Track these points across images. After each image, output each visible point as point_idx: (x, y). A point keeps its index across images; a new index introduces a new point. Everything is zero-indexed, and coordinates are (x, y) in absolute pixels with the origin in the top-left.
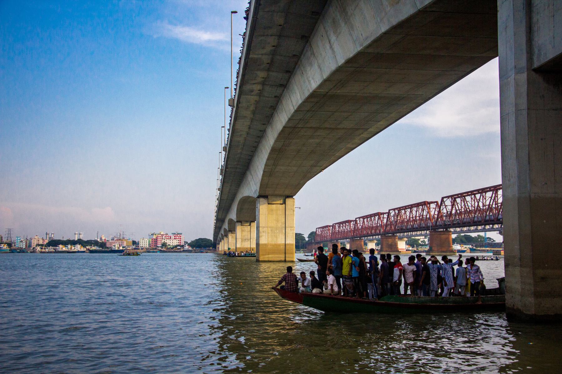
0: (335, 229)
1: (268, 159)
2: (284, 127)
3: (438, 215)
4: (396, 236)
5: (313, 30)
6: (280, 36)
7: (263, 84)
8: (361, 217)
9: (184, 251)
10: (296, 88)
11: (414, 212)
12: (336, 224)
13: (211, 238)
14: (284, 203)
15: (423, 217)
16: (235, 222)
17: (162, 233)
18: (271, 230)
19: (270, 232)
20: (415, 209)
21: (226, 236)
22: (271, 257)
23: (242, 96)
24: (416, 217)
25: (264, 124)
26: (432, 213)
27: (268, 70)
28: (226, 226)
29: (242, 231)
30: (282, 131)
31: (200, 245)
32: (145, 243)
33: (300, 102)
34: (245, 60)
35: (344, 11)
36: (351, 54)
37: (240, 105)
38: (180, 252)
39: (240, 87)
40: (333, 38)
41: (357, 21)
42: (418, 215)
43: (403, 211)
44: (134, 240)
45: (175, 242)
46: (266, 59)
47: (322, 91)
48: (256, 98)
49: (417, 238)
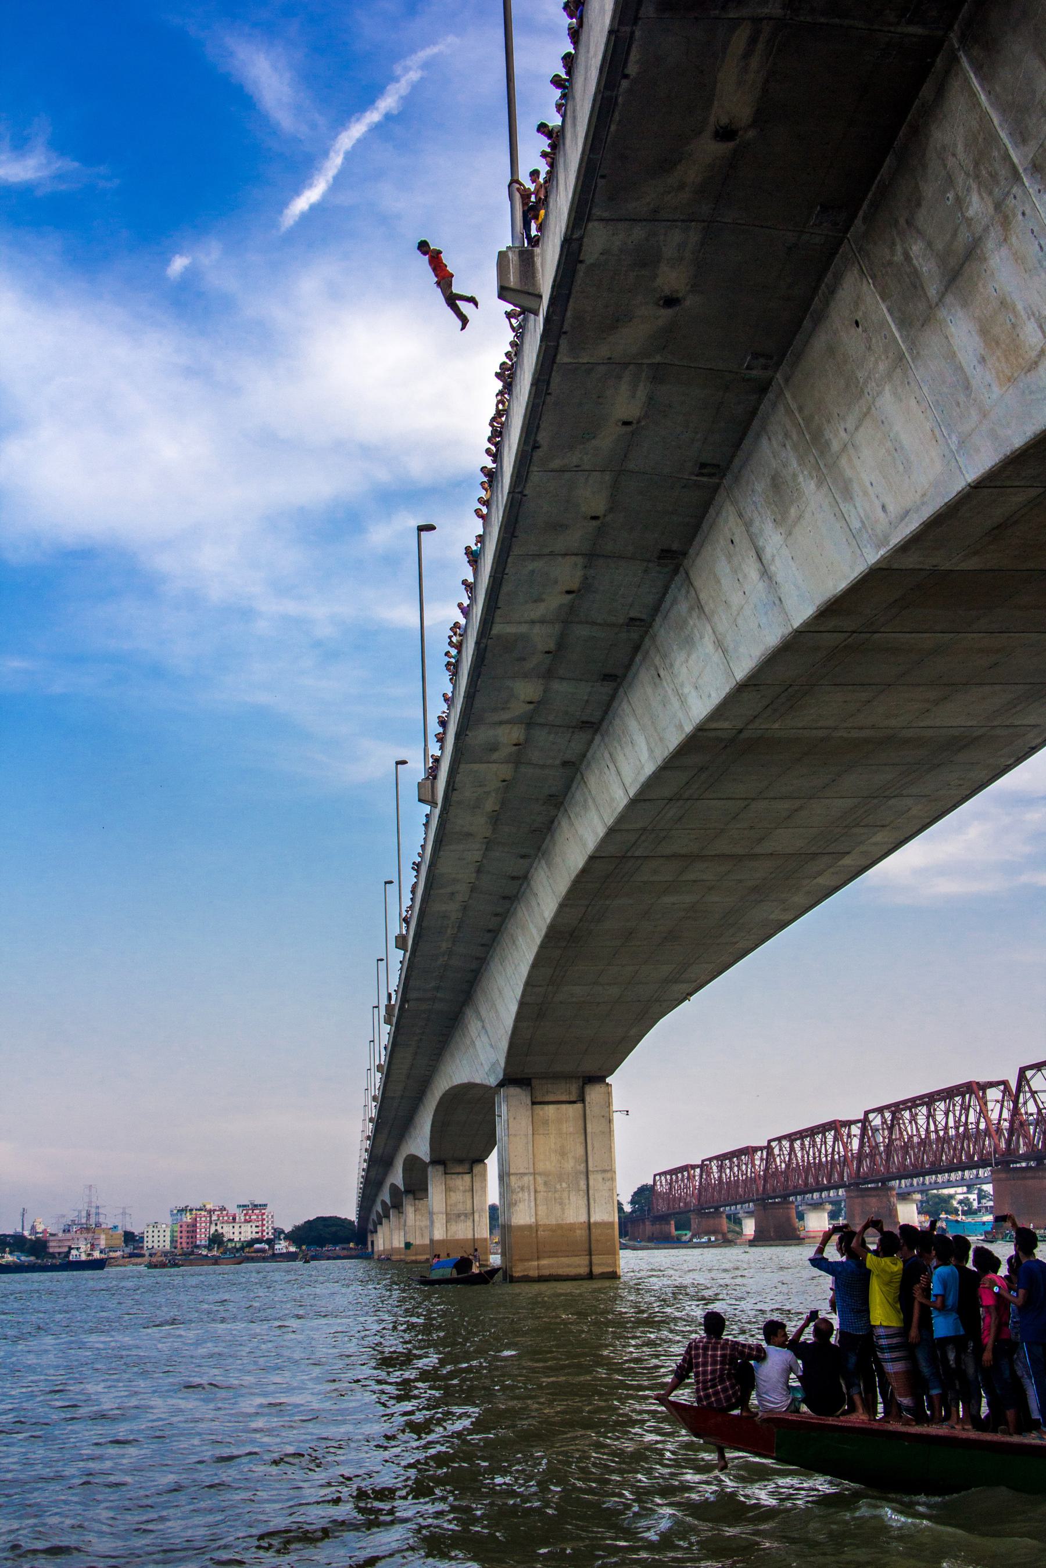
0: (709, 1174)
1: (534, 966)
2: (592, 858)
3: (1012, 1122)
4: (892, 1188)
5: (696, 528)
6: (591, 557)
7: (529, 722)
8: (784, 1137)
9: (276, 1257)
10: (633, 725)
11: (940, 1117)
12: (710, 1159)
13: (350, 1212)
14: (582, 1099)
15: (966, 1129)
16: (425, 1165)
17: (208, 1207)
18: (545, 1183)
19: (541, 1188)
20: (942, 1105)
21: (398, 1206)
22: (547, 1265)
23: (463, 767)
24: (946, 1128)
25: (523, 857)
26: (994, 1116)
27: (548, 675)
28: (397, 1177)
29: (448, 1190)
30: (584, 871)
31: (320, 1238)
32: (159, 1240)
33: (649, 769)
34: (477, 643)
35: (815, 443)
36: (839, 582)
37: (455, 797)
38: (264, 1259)
39: (458, 736)
40: (772, 540)
41: (865, 464)
42: (951, 1123)
43: (907, 1114)
44: (129, 1229)
45: (247, 1232)
46: (543, 637)
47: (726, 725)
48: (506, 771)
49: (946, 1191)
